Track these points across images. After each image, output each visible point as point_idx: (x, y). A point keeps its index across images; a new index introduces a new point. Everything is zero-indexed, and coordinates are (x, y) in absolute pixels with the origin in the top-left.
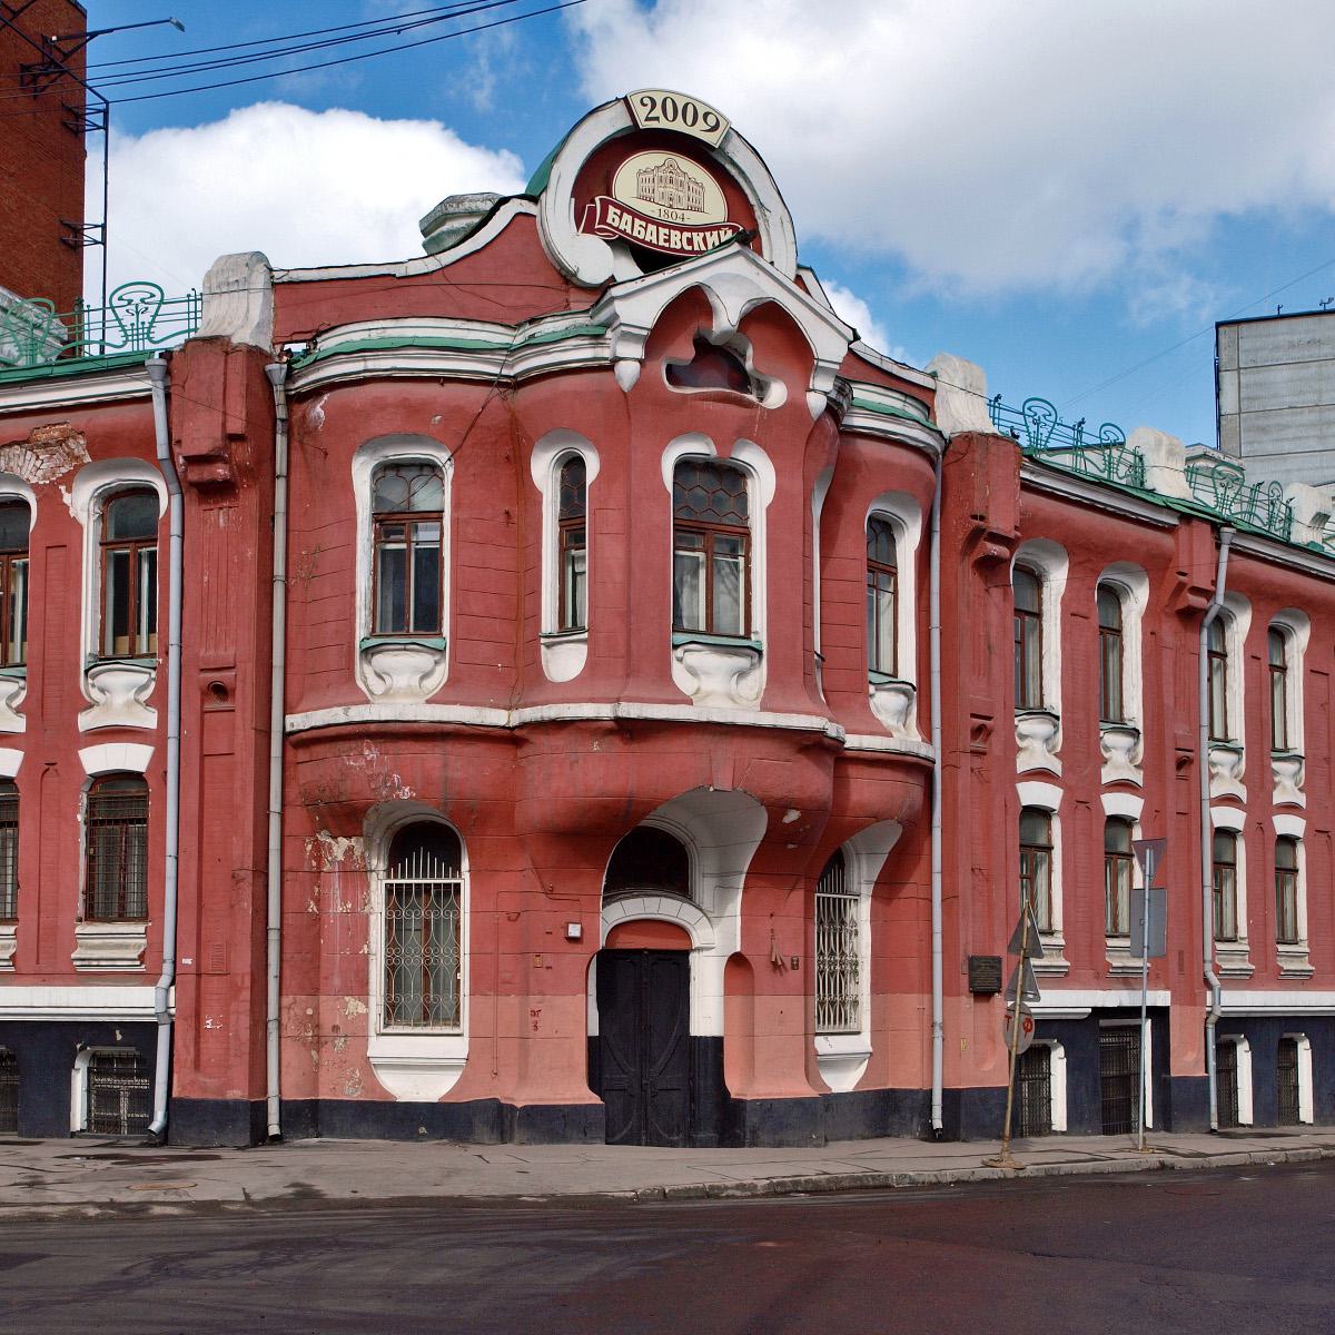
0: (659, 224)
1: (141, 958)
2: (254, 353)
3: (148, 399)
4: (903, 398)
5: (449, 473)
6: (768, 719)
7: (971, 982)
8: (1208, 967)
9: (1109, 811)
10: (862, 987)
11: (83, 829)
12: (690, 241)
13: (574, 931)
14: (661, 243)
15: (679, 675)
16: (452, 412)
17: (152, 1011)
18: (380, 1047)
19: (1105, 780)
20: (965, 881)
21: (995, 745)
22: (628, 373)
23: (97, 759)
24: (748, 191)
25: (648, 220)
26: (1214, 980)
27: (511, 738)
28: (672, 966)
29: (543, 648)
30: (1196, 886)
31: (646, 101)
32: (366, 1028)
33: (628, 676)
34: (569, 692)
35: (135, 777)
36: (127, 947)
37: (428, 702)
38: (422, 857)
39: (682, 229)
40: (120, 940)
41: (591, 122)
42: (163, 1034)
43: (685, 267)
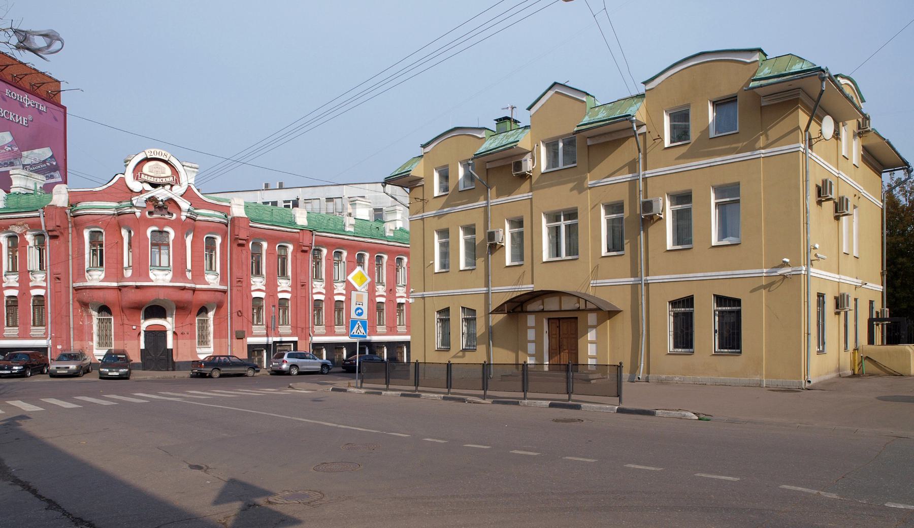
2: (63, 208)
3: (39, 217)
5: (104, 234)
6: (716, 136)
9: (280, 297)
10: (211, 337)
11: (32, 307)
12: (162, 180)
13: (134, 327)
15: (151, 275)
18: (198, 350)
19: (279, 290)
20: (235, 315)
21: (244, 285)
23: (34, 292)
25: (152, 176)
27: (119, 288)
28: (163, 333)
29: (124, 270)
30: (307, 315)
32: (93, 348)
33: (140, 276)
34: (129, 280)
35: (42, 296)
40: (39, 330)
41: (116, 176)
42: (49, 350)
43: (149, 193)
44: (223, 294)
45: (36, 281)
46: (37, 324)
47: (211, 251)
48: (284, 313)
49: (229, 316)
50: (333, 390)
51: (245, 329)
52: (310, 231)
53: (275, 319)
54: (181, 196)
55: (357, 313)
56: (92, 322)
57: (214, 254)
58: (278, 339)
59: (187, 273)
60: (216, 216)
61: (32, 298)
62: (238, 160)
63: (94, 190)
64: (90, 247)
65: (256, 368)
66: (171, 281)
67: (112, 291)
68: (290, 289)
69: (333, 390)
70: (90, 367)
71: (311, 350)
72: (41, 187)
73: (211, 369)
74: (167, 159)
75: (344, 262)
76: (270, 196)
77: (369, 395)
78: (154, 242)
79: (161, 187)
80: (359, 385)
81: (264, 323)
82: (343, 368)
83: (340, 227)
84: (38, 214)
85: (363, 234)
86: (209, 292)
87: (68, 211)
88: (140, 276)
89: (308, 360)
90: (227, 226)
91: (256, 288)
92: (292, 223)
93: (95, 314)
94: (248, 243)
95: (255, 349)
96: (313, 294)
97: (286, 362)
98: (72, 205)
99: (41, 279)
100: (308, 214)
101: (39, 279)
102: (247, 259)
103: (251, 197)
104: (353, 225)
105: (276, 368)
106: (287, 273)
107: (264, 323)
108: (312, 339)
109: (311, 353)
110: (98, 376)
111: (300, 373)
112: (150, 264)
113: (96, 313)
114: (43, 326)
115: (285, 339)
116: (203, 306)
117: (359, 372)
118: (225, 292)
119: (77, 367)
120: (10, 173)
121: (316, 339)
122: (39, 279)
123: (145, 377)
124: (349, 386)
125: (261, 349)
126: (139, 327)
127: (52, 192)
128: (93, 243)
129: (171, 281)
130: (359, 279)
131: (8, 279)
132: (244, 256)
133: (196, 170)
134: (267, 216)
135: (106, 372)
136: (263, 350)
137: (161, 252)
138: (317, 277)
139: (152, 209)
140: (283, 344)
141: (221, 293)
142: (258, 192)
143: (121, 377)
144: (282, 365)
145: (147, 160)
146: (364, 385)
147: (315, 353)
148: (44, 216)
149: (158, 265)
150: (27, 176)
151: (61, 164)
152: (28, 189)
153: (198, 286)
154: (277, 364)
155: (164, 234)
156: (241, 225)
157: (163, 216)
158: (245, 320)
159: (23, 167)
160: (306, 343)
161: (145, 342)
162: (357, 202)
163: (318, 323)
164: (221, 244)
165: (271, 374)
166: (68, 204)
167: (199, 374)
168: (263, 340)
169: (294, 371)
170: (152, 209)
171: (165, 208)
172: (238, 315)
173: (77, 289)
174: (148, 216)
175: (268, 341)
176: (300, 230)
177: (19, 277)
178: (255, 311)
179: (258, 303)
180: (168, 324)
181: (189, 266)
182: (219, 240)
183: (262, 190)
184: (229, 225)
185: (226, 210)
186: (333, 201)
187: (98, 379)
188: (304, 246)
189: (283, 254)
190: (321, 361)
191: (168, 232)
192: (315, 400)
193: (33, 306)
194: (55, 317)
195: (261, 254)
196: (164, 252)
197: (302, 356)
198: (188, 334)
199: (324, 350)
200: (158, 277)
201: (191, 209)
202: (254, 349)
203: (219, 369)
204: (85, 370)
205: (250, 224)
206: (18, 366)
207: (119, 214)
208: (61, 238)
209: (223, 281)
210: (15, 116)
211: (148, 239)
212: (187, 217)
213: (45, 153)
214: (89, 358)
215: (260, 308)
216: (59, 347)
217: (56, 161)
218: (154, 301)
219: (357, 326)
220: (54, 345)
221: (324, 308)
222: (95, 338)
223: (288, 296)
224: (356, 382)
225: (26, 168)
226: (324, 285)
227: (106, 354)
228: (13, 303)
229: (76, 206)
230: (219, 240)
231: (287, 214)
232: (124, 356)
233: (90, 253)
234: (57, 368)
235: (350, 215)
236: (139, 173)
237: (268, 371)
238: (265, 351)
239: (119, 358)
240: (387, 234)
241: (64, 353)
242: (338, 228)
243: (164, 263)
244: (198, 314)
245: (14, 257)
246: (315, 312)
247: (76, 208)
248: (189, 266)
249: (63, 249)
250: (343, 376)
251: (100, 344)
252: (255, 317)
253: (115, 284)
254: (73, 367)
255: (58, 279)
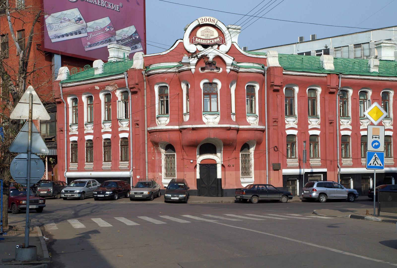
0: (205, 39)
1: (128, 167)
3: (124, 78)
4: (253, 64)
6: (219, 126)
7: (273, 168)
8: (338, 163)
9: (310, 134)
10: (252, 169)
11: (120, 147)
12: (211, 42)
13: (192, 161)
14: (206, 43)
15: (204, 119)
16: (168, 78)
17: (129, 175)
18: (242, 180)
19: (286, 128)
20: (272, 150)
21: (279, 124)
22: (193, 71)
23: (122, 135)
24: (222, 31)
25: (203, 39)
26: (339, 166)
27: (180, 130)
28: (213, 166)
29: (184, 116)
30: (335, 148)
31: (201, 19)
33: (195, 120)
34: (188, 123)
36: (126, 165)
37: (166, 126)
38: (170, 150)
39: (209, 40)
40: (123, 164)
42: (131, 179)
44: (262, 132)
45: (123, 127)
46: (123, 159)
47: (252, 97)
48: (315, 147)
49: (267, 151)
50: (352, 217)
51: (280, 162)
52: (337, 74)
53: (306, 152)
54: (226, 53)
55: (374, 146)
56: (161, 157)
57: (253, 99)
58: (309, 170)
59: (232, 116)
60: (254, 67)
61: (120, 140)
62: (251, 14)
63: (161, 54)
64: (159, 99)
65: (288, 195)
66: (219, 123)
67: (175, 132)
68: (319, 127)
69: (352, 217)
70: (159, 193)
71: (340, 180)
72: (128, 56)
73: (251, 196)
74: (214, 24)
75: (369, 100)
76: (304, 48)
77: (385, 223)
78: (206, 92)
79: (210, 47)
80: (376, 213)
81: (297, 156)
82: (369, 197)
83: (365, 68)
84: (124, 76)
85: (387, 74)
86: (250, 132)
87: (143, 72)
88: (195, 120)
89: (335, 189)
90: (264, 75)
91: (290, 127)
92: (321, 69)
93: (163, 151)
94: (282, 88)
95: (289, 179)
96: (340, 130)
97: (316, 190)
98: (146, 67)
99: (126, 125)
100: (336, 60)
101: (124, 125)
102: (282, 102)
103: (286, 50)
104: (377, 66)
105: (308, 196)
106: (316, 113)
107: (297, 156)
108: (340, 170)
109: (339, 183)
110: (164, 200)
111: (328, 201)
112: (203, 110)
113: (164, 151)
114: (92, 162)
115: (315, 170)
116: (246, 143)
117: (376, 200)
118: (263, 131)
119: (149, 192)
120: (108, 48)
121: (344, 170)
122: (124, 125)
123: (199, 201)
124: (367, 214)
125: (294, 179)
126: (195, 161)
127: (133, 58)
128: (161, 96)
129: (219, 123)
130: (375, 114)
131: (105, 126)
132: (278, 100)
133: (239, 31)
134: (298, 64)
135: (170, 197)
136: (296, 180)
137: (212, 100)
138: (344, 115)
139: (204, 65)
140: (314, 175)
141: (259, 132)
142: (294, 45)
143: (180, 201)
144: (312, 193)
145: (200, 26)
146: (381, 213)
147: (343, 183)
148: (127, 77)
149: (209, 110)
150: (119, 49)
151: (142, 38)
152: (119, 58)
153: (241, 127)
154: (308, 192)
155: (213, 85)
156: (275, 74)
157: (212, 71)
158: (281, 154)
159: (117, 43)
160: (334, 174)
161: (201, 173)
162: (382, 45)
163: (345, 156)
164: (259, 91)
165: (303, 201)
166: (144, 67)
167: (241, 200)
168: (296, 171)
169: (323, 199)
170: (204, 65)
171: (214, 64)
172: (275, 150)
173: (150, 132)
174: (201, 72)
175: (300, 172)
176: (328, 74)
177: (112, 124)
178: (289, 146)
179: (291, 139)
180: (218, 158)
181: (233, 111)
182: (257, 88)
183: (298, 43)
184: (266, 74)
185: (262, 62)
186: (361, 47)
187: (164, 203)
188: (331, 88)
189: (312, 96)
190: (347, 190)
191: (216, 84)
192: (330, 226)
193: (121, 146)
194: (135, 154)
195: (294, 97)
196: (213, 100)
197: (331, 185)
198: (233, 166)
199: (351, 180)
200: (209, 121)
201: (234, 63)
202: (288, 179)
203: (258, 196)
204: (155, 195)
205: (283, 72)
206: (110, 191)
207: (179, 72)
208: (139, 93)
209: (261, 121)
210: (111, 5)
211: (202, 90)
212: (231, 70)
213: (130, 30)
214: (158, 185)
215: (293, 144)
216: (138, 177)
217: (138, 35)
218: (207, 140)
219: (374, 158)
220: (135, 175)
221: (351, 143)
222: (163, 170)
223: (318, 133)
224: (373, 210)
225: (119, 43)
226: (350, 122)
227: (170, 183)
228: (108, 143)
229: (149, 68)
230: (257, 88)
231: (315, 61)
232: (183, 185)
233: (159, 103)
234: (135, 193)
235: (376, 57)
236: (194, 37)
237: (301, 199)
238: (298, 181)
239: (180, 186)
240: (372, 70)
241: (140, 181)
242: (363, 69)
243: (214, 109)
244: (242, 150)
245: (109, 110)
246: (343, 146)
247: (149, 70)
248: (233, 111)
249: (140, 101)
250: (367, 204)
251: (167, 175)
252: (343, 151)
253: (177, 127)
254: (146, 193)
255: (138, 124)
